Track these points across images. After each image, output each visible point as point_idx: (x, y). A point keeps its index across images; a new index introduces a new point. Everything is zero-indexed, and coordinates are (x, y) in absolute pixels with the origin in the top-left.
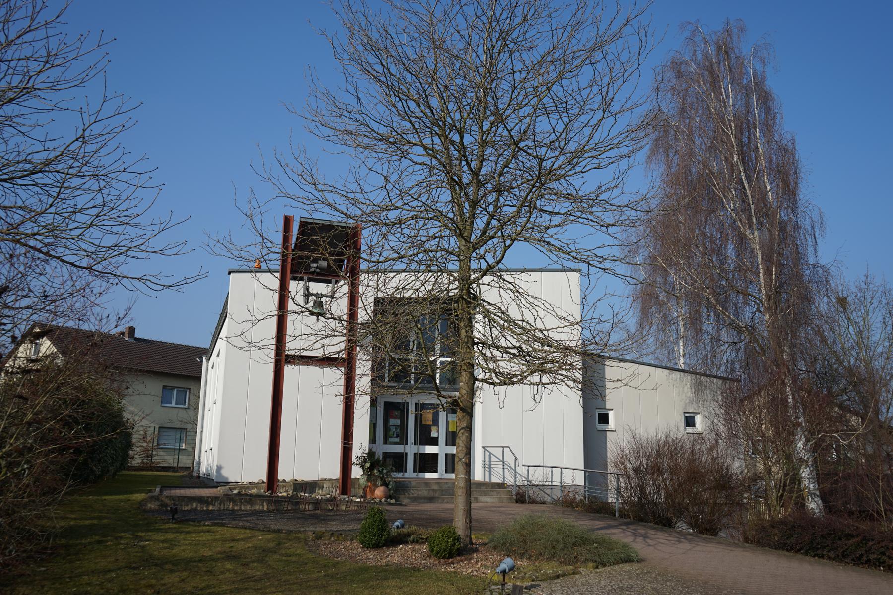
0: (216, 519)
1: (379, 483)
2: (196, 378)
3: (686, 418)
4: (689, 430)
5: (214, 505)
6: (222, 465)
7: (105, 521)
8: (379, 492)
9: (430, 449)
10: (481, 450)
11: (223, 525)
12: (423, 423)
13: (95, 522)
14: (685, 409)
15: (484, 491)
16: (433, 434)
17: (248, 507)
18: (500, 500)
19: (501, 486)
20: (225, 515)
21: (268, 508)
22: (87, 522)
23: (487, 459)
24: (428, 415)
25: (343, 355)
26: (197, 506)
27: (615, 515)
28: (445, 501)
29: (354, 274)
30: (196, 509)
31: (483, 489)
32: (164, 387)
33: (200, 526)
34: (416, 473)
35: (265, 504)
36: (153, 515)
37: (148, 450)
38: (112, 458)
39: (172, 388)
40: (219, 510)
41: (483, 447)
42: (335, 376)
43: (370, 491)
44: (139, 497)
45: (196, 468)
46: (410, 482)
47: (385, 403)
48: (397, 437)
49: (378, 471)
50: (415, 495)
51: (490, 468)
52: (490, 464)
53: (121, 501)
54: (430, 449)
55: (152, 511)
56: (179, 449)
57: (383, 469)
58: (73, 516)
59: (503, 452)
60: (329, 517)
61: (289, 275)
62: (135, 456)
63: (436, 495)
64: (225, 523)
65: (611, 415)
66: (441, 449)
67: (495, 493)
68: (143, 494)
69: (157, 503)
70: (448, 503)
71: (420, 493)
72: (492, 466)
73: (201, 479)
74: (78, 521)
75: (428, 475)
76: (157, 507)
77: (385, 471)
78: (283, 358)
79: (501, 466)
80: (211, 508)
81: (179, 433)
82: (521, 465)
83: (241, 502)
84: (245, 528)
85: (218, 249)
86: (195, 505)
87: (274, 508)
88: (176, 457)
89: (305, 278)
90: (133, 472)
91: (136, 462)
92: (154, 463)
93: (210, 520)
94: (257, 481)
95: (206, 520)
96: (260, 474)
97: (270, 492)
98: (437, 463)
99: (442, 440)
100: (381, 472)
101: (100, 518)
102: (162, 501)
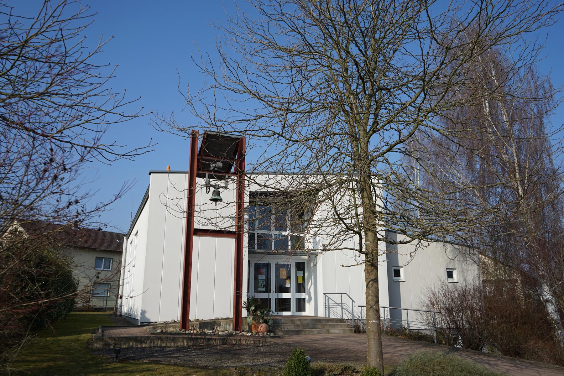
0: (151, 357)
1: (261, 321)
2: (119, 252)
3: (448, 272)
4: (450, 280)
5: (146, 343)
6: (146, 310)
7: (60, 362)
8: (262, 327)
9: (285, 296)
10: (323, 296)
11: (158, 363)
12: (281, 277)
13: (52, 364)
14: (447, 266)
15: (332, 325)
16: (288, 285)
17: (172, 344)
18: (344, 331)
19: (342, 321)
20: (156, 352)
21: (187, 345)
22: (45, 365)
23: (327, 302)
24: (283, 273)
25: (233, 229)
26: (133, 344)
27: (434, 342)
28: (307, 333)
29: (240, 173)
30: (132, 347)
31: (330, 323)
32: (97, 258)
33: (139, 364)
34: (277, 312)
35: (185, 341)
36: (99, 354)
37: (87, 298)
38: (64, 305)
39: (102, 258)
40: (150, 347)
41: (324, 294)
42: (231, 242)
43: (255, 327)
44: (86, 336)
45: (119, 310)
46: (281, 320)
47: (255, 264)
48: (263, 288)
49: (261, 312)
50: (286, 329)
51: (329, 308)
52: (329, 305)
53: (72, 341)
54: (285, 296)
55: (98, 350)
56: (107, 297)
57: (264, 311)
58: (34, 358)
59: (341, 297)
60: (238, 352)
61: (195, 172)
62: (79, 302)
63: (300, 329)
64: (160, 361)
65: (402, 271)
66: (293, 296)
67: (339, 326)
68: (89, 334)
69: (102, 343)
70: (309, 334)
71: (289, 327)
72: (330, 306)
73: (122, 317)
74: (37, 364)
75: (285, 313)
76: (101, 347)
77: (265, 312)
78: (192, 232)
79: (330, 304)
80: (144, 345)
81: (107, 286)
82: (357, 306)
83: (167, 340)
84: (177, 365)
85: (164, 126)
86: (131, 343)
87: (191, 344)
88: (105, 302)
89: (207, 175)
90: (77, 313)
91: (79, 305)
92: (91, 306)
93: (146, 358)
94: (170, 321)
95: (144, 358)
96: (178, 317)
97: (184, 330)
98: (290, 304)
99: (293, 288)
100: (263, 313)
101: (54, 360)
102: (105, 341)
